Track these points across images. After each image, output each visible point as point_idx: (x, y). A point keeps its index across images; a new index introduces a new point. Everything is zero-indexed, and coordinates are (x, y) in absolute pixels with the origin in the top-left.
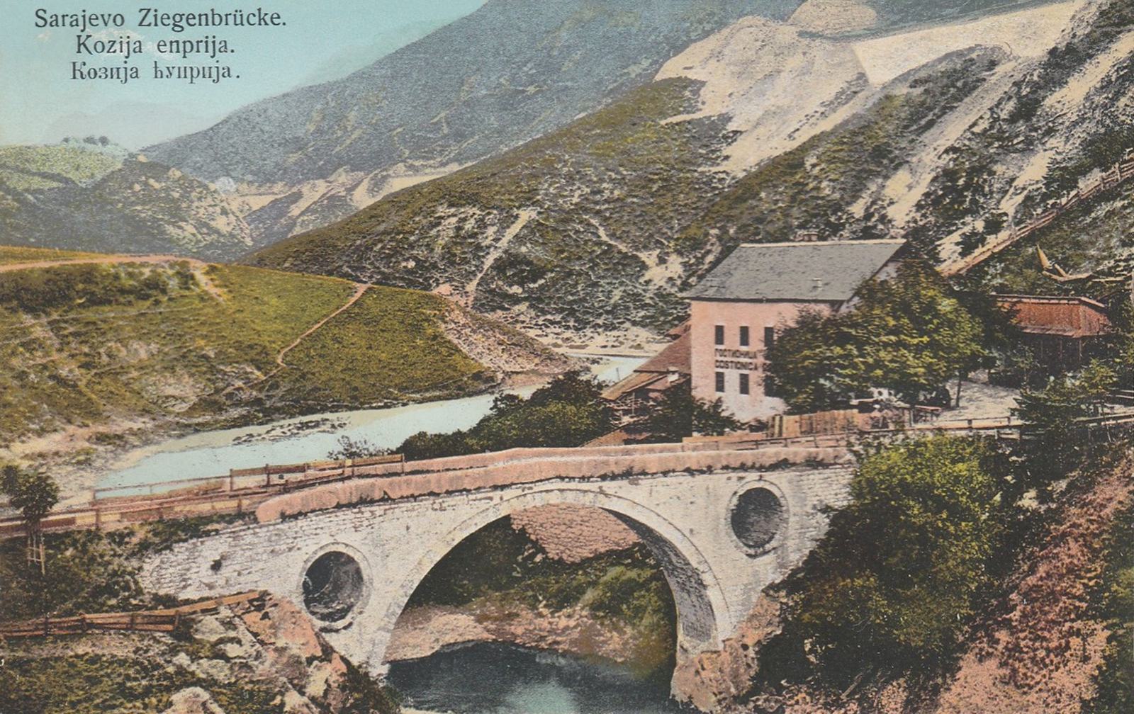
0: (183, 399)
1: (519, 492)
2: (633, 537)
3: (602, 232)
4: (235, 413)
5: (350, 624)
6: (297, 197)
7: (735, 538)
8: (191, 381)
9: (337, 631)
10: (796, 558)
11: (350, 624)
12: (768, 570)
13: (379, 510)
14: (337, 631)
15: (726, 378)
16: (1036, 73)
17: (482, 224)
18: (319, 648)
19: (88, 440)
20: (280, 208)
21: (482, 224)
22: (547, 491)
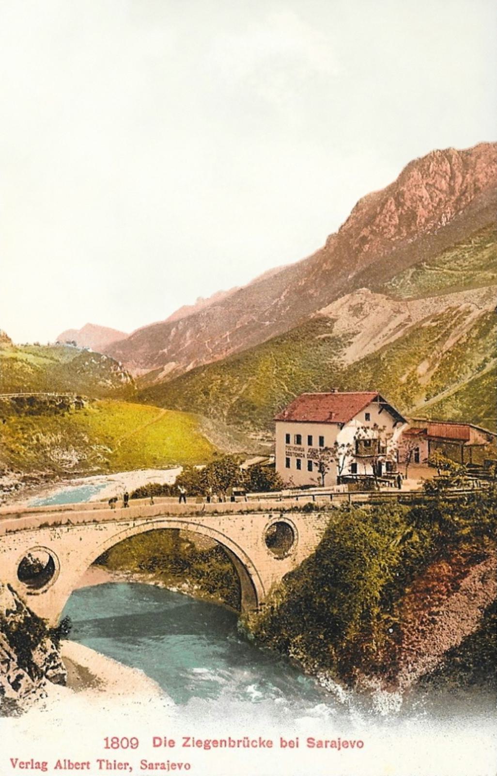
0: (70, 462)
1: (145, 521)
2: (217, 544)
3: (286, 388)
4: (96, 468)
5: (46, 591)
6: (163, 369)
7: (267, 548)
8: (76, 453)
9: (38, 594)
10: (299, 561)
11: (46, 591)
12: (286, 566)
13: (65, 529)
14: (38, 594)
15: (302, 462)
16: (489, 316)
17: (232, 384)
18: (15, 606)
19: (19, 480)
20: (154, 373)
21: (232, 384)
22: (161, 521)
